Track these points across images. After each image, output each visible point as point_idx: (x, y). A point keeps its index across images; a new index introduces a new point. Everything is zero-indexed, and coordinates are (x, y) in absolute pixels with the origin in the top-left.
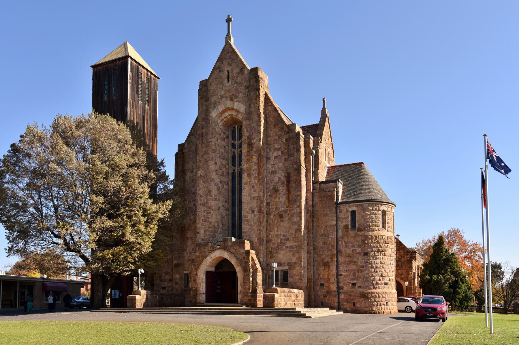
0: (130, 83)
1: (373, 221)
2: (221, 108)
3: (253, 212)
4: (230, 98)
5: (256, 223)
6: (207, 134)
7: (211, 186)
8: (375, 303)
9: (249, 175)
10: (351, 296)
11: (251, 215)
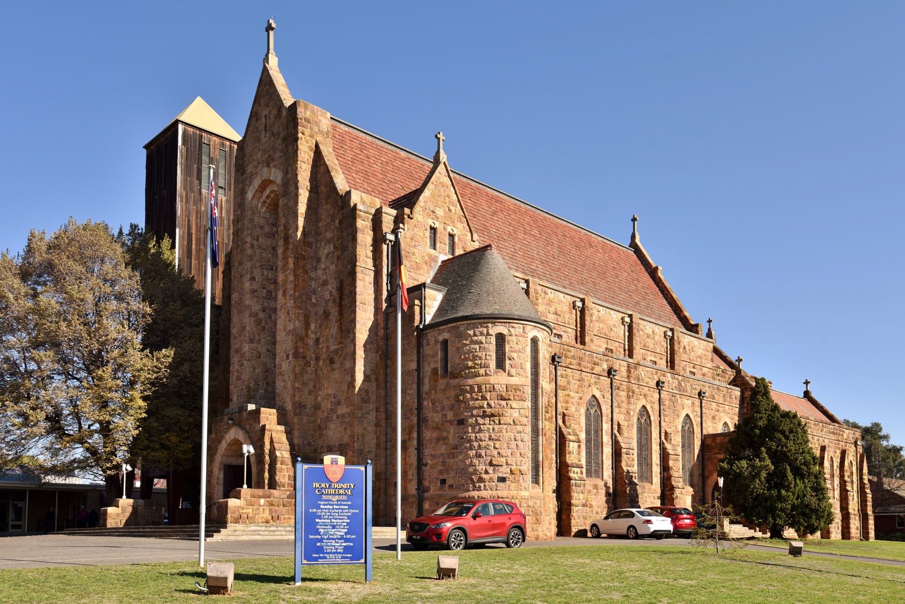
0: (181, 164)
1: (475, 357)
2: (257, 182)
10: (437, 505)
11: (286, 363)
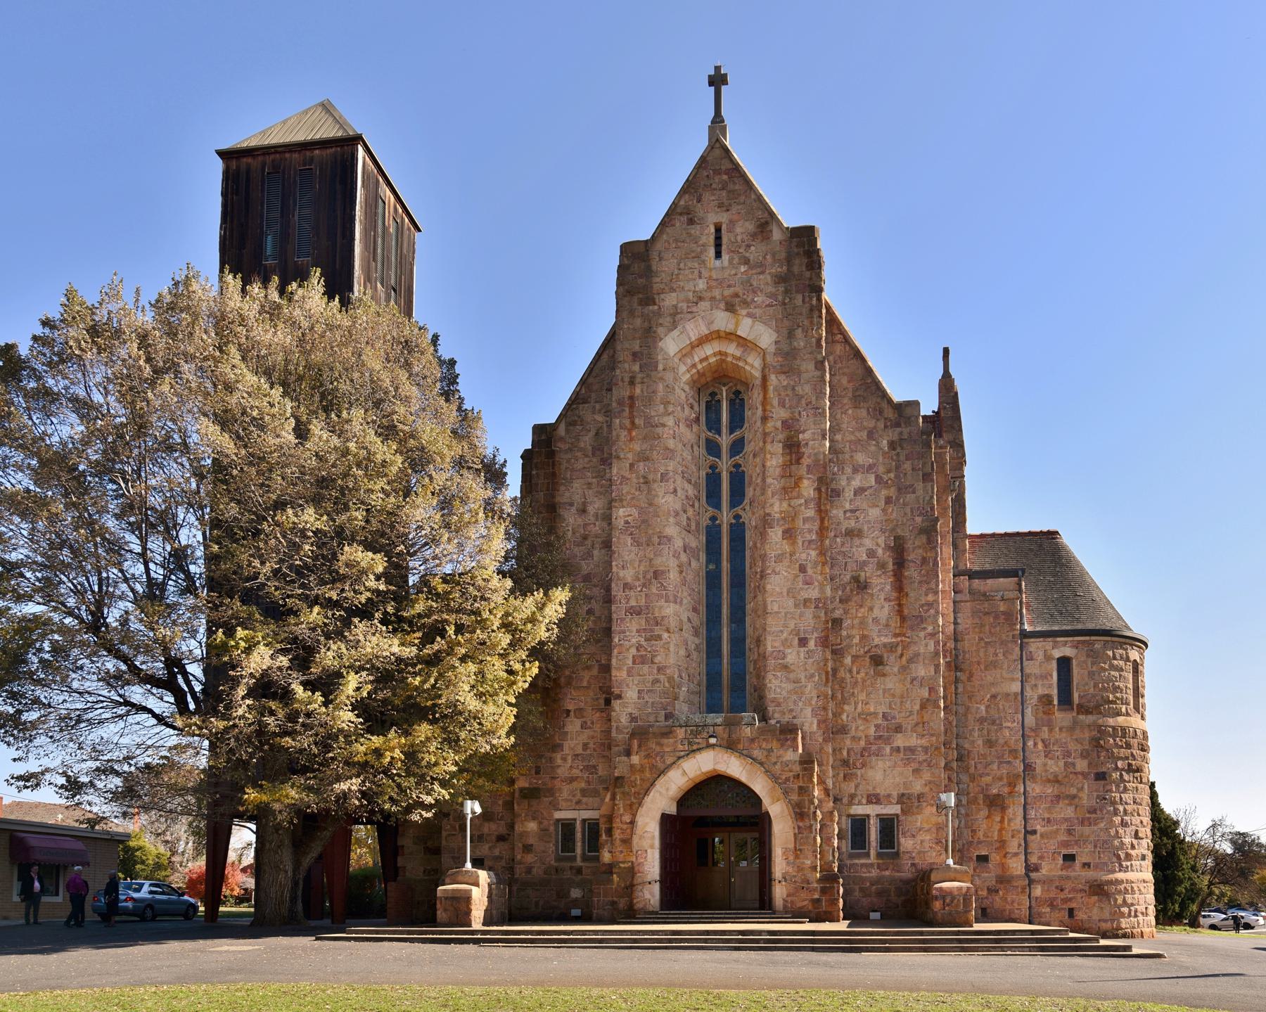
0: (360, 221)
2: (694, 329)
3: (803, 642)
4: (726, 304)
5: (812, 676)
6: (649, 401)
7: (664, 559)
8: (1125, 910)
9: (789, 534)
